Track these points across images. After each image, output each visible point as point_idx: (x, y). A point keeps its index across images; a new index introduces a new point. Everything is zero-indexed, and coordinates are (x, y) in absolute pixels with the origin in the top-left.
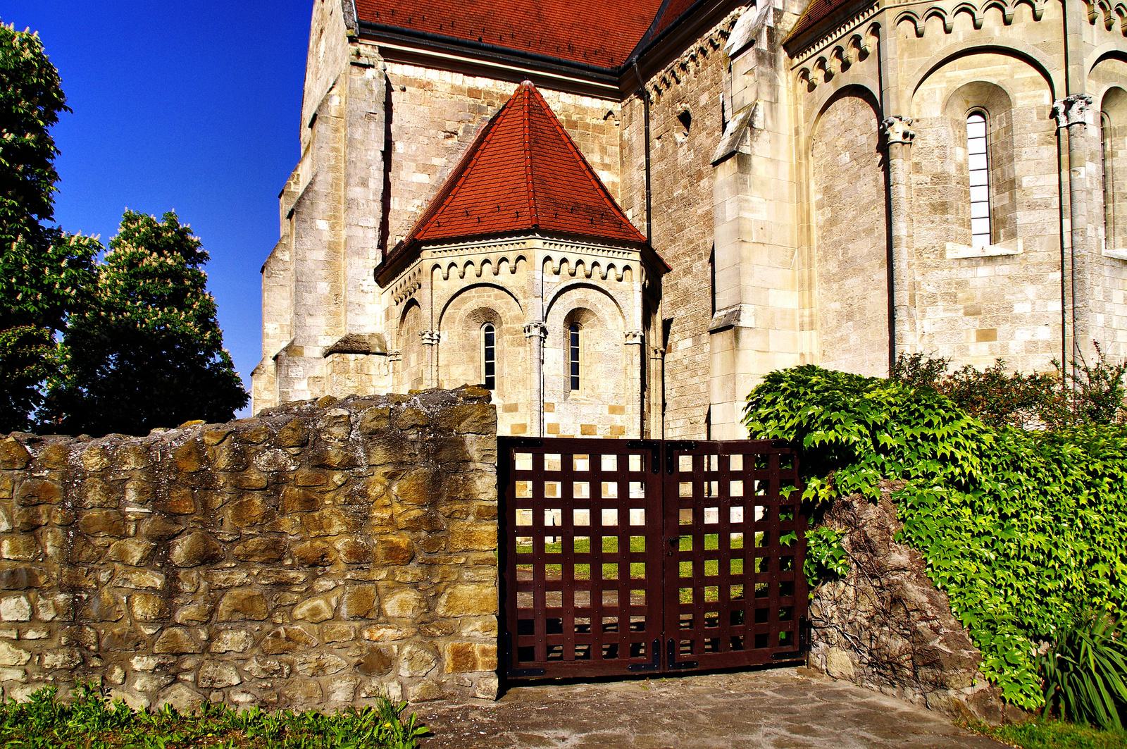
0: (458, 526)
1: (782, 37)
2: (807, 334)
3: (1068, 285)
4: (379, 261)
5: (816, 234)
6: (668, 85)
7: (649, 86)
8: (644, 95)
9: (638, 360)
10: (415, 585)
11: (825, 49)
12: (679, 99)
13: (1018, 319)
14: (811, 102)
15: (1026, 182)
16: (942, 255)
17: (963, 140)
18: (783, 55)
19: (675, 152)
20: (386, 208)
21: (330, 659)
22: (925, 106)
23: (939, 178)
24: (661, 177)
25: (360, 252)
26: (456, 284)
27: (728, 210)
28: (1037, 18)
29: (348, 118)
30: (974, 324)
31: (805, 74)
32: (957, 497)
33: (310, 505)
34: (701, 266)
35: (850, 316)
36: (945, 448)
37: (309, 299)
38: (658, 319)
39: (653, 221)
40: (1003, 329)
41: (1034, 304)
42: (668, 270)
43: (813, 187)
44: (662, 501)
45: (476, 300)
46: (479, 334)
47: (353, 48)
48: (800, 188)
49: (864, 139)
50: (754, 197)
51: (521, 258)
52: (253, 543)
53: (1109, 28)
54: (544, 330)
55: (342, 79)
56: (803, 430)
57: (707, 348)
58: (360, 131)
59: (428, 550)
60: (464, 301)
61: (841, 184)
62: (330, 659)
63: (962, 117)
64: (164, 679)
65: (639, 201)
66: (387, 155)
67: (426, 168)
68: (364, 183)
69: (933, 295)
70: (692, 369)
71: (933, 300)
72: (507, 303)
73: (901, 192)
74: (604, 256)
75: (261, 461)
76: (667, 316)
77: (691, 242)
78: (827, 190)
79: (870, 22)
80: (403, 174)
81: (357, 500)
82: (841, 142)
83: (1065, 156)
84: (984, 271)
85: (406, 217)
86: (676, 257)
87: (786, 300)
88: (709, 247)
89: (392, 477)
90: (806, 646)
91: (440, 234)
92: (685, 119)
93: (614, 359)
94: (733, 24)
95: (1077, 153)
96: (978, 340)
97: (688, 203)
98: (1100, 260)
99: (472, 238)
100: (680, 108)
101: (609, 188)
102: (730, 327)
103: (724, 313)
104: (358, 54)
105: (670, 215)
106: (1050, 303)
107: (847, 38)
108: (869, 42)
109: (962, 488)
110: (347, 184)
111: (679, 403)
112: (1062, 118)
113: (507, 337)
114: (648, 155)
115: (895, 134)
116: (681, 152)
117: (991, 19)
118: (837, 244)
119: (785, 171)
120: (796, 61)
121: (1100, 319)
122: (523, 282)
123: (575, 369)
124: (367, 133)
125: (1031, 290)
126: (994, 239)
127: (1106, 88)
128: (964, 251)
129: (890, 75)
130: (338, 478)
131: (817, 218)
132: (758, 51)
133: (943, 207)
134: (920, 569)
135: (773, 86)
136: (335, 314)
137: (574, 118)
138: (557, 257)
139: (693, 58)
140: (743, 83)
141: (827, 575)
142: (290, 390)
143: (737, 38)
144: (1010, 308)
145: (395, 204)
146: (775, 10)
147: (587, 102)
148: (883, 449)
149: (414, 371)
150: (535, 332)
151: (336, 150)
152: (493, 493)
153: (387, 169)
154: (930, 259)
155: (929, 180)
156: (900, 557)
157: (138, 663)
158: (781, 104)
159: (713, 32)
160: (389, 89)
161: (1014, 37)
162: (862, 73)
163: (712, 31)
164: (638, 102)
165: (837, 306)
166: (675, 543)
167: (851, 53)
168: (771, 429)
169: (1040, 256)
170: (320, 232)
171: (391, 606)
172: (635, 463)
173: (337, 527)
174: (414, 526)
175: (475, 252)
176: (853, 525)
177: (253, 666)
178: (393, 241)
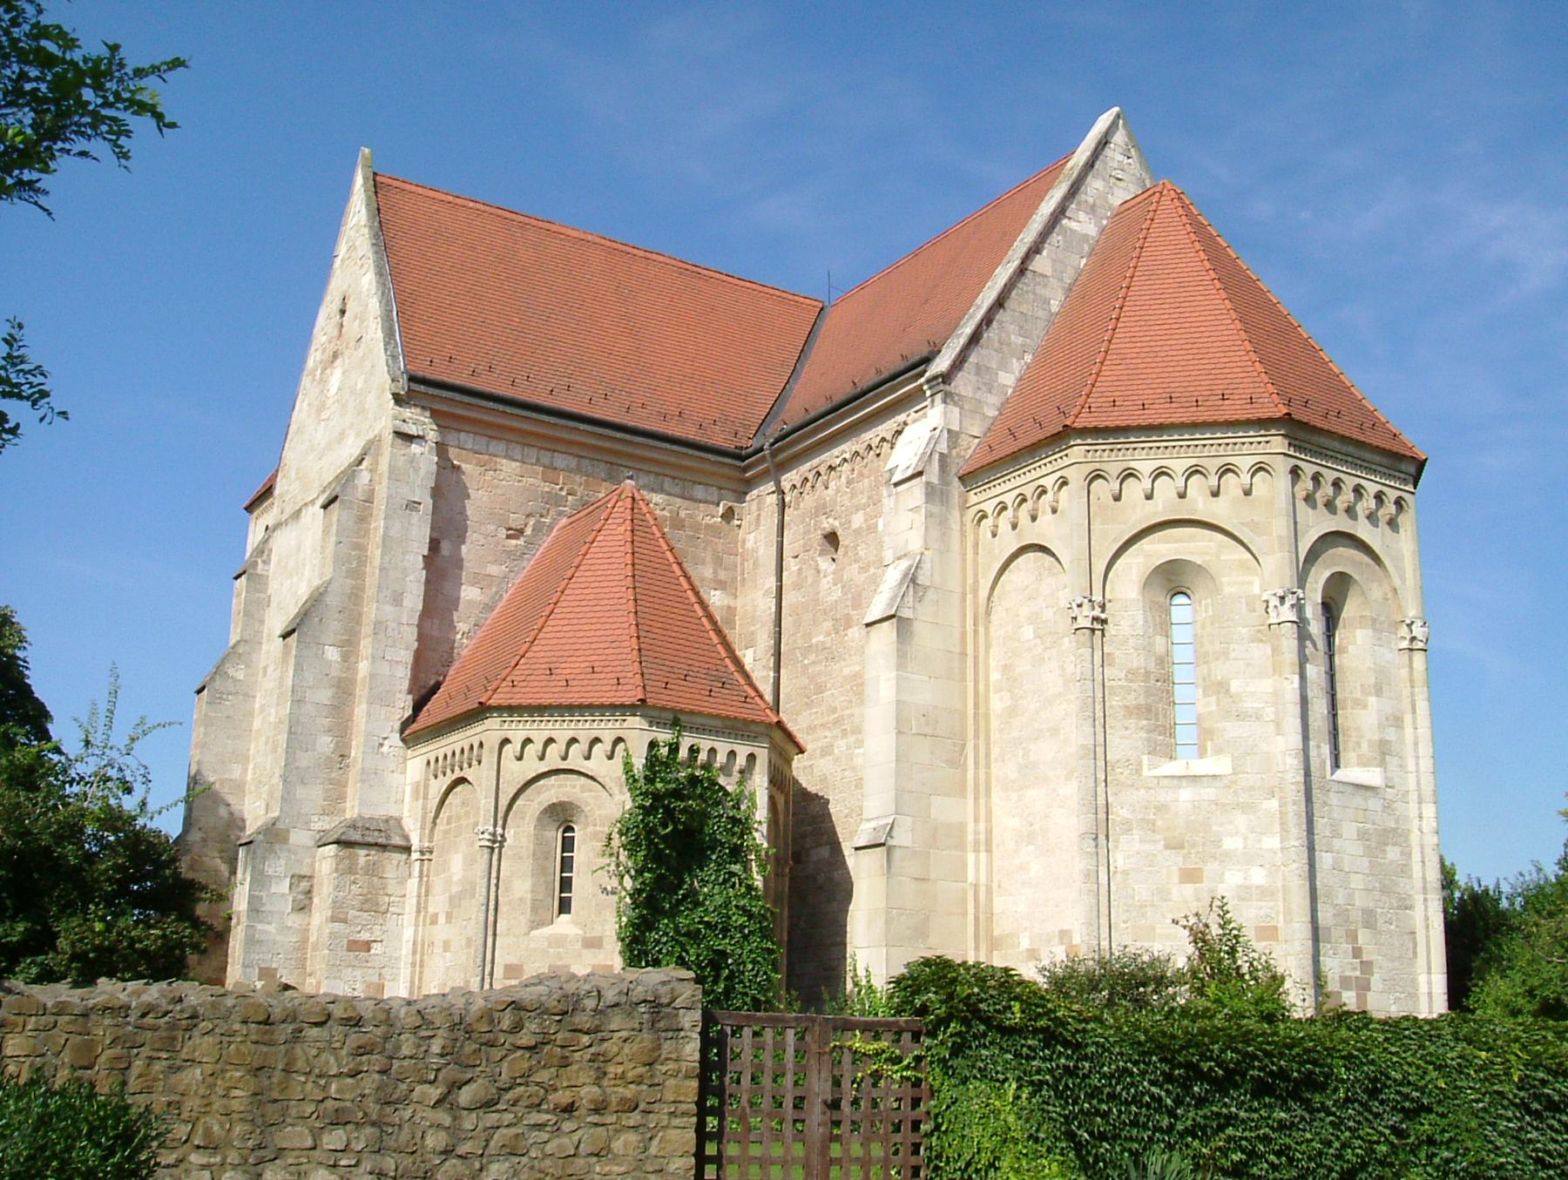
1: (958, 466)
12: (823, 509)
13: (1227, 856)
19: (816, 582)
40: (1210, 868)
41: (1245, 839)
51: (619, 740)
58: (398, 525)
65: (765, 641)
69: (1128, 821)
71: (1128, 827)
72: (596, 798)
77: (834, 710)
79: (1059, 474)
82: (1024, 611)
92: (832, 538)
96: (1182, 882)
100: (827, 524)
103: (873, 824)
105: (806, 667)
106: (1264, 838)
116: (825, 583)
125: (1241, 821)
142: (263, 894)
144: (1218, 843)
146: (949, 431)
152: (697, 1056)
155: (1123, 675)
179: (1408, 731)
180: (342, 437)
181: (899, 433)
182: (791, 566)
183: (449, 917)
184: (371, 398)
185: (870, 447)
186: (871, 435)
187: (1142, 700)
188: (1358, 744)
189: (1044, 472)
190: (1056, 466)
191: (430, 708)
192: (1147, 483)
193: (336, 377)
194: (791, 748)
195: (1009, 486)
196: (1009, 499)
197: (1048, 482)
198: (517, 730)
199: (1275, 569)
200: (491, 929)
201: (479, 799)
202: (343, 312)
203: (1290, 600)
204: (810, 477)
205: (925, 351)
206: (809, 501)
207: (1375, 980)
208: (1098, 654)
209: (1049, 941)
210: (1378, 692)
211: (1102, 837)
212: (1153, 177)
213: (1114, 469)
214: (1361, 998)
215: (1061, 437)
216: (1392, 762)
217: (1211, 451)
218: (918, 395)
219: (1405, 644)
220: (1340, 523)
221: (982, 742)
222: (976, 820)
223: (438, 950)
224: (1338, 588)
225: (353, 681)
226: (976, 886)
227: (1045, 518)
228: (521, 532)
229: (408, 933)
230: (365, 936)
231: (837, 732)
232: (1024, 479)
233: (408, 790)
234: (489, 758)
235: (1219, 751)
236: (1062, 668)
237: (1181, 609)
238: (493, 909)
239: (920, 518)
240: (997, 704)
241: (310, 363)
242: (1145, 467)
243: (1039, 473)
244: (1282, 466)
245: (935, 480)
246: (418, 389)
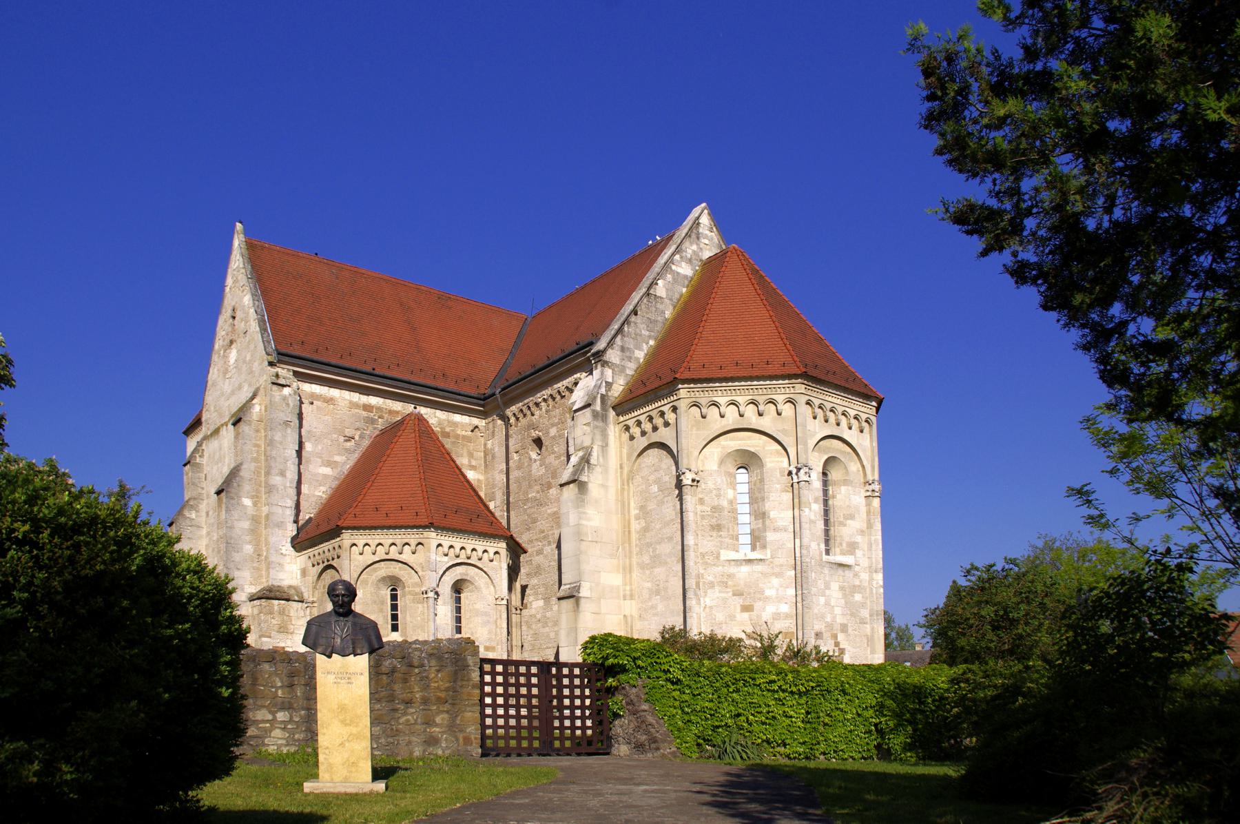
0: (465, 690)
2: (628, 602)
3: (799, 580)
4: (295, 533)
5: (634, 536)
6: (525, 416)
7: (509, 412)
8: (505, 419)
9: (505, 616)
10: (447, 712)
11: (641, 413)
12: (533, 426)
14: (631, 448)
15: (773, 514)
16: (718, 557)
17: (733, 485)
18: (612, 413)
19: (530, 465)
20: (299, 493)
21: (414, 739)
22: (707, 463)
23: (716, 509)
24: (518, 481)
25: (280, 525)
27: (572, 518)
28: (779, 414)
29: (268, 423)
30: (738, 601)
31: (627, 428)
32: (670, 686)
33: (405, 681)
34: (551, 550)
35: (658, 593)
36: (666, 667)
38: (518, 586)
39: (512, 513)
43: (632, 504)
44: (545, 686)
45: (384, 570)
46: (387, 593)
47: (273, 370)
48: (624, 506)
49: (667, 478)
50: (590, 511)
52: (382, 694)
53: (826, 421)
54: (437, 593)
55: (261, 392)
56: (607, 658)
57: (555, 608)
58: (279, 434)
59: (452, 699)
60: (375, 570)
61: (651, 506)
62: (414, 739)
63: (732, 469)
66: (299, 453)
67: (329, 464)
68: (282, 474)
69: (712, 583)
70: (544, 622)
71: (712, 585)
73: (690, 517)
74: (480, 545)
75: (387, 663)
76: (524, 583)
78: (642, 508)
80: (311, 467)
81: (425, 681)
82: (652, 478)
83: (796, 500)
84: (745, 569)
85: (314, 499)
86: (531, 541)
87: (614, 579)
88: (557, 537)
89: (438, 671)
90: (610, 746)
91: (356, 523)
92: (538, 442)
93: (486, 614)
94: (576, 384)
95: (803, 499)
97: (540, 504)
98: (821, 564)
99: (382, 528)
100: (535, 434)
101: (474, 484)
102: (572, 596)
104: (277, 376)
107: (656, 411)
108: (670, 417)
109: (673, 683)
110: (268, 473)
111: (533, 645)
112: (795, 477)
113: (409, 597)
114: (507, 464)
115: (687, 479)
117: (750, 411)
118: (649, 545)
119: (612, 493)
120: (621, 419)
121: (822, 600)
122: (421, 560)
123: (458, 620)
124: (284, 437)
125: (775, 581)
126: (753, 549)
127: (826, 457)
128: (733, 555)
129: (684, 441)
130: (417, 671)
131: (635, 526)
132: (594, 411)
133: (718, 527)
134: (653, 712)
135: (605, 436)
136: (258, 569)
137: (448, 430)
138: (446, 544)
139: (545, 400)
140: (582, 431)
141: (616, 716)
143: (578, 398)
144: (762, 592)
145: (305, 489)
147: (458, 418)
148: (639, 667)
150: (431, 594)
151: (258, 446)
153: (300, 463)
154: (710, 559)
156: (645, 707)
158: (612, 447)
159: (561, 385)
160: (301, 403)
161: (765, 423)
162: (665, 435)
163: (559, 385)
164: (499, 422)
165: (649, 585)
166: (551, 702)
167: (659, 421)
168: (591, 658)
169: (782, 561)
170: (245, 507)
171: (438, 720)
173: (416, 689)
174: (447, 690)
176: (626, 696)
177: (382, 740)
178: (304, 516)
180: (240, 387)
193: (233, 355)
202: (234, 318)
217: (761, 390)
227: (662, 430)
241: (216, 347)
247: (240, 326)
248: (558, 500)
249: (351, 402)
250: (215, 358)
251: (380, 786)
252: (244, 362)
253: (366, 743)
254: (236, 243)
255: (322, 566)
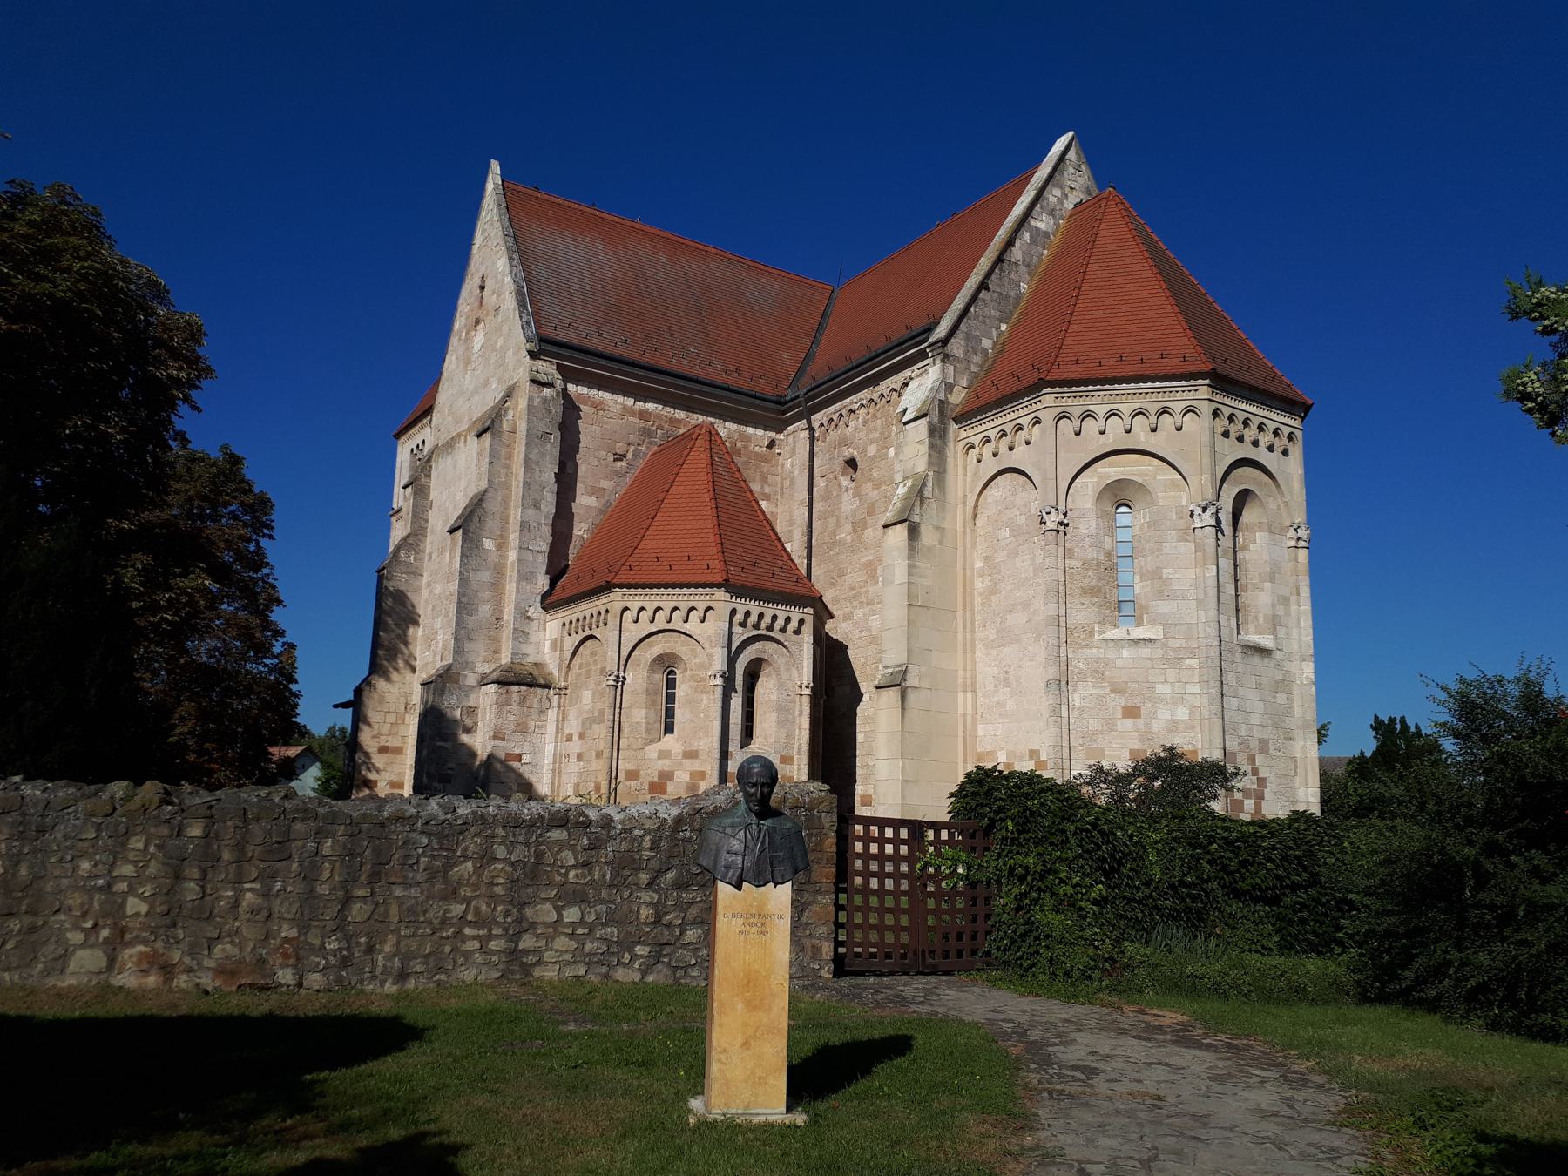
4: (546, 588)
12: (844, 442)
24: (822, 518)
26: (645, 628)
35: (1006, 683)
37: (471, 622)
42: (832, 617)
46: (660, 678)
51: (709, 608)
60: (651, 645)
64: (652, 961)
78: (987, 559)
92: (852, 463)
100: (848, 453)
107: (1288, 430)
149: (587, 708)
152: (834, 849)
157: (639, 950)
172: (904, 834)
175: (666, 600)
179: (1293, 608)
180: (486, 383)
181: (906, 385)
182: (820, 484)
183: (581, 736)
184: (510, 353)
185: (882, 396)
186: (885, 386)
187: (1094, 583)
188: (1256, 618)
189: (1021, 413)
190: (1031, 409)
191: (566, 582)
192: (1101, 421)
193: (479, 338)
194: (825, 615)
195: (992, 424)
196: (992, 434)
197: (1024, 421)
198: (635, 600)
199: (1202, 483)
200: (616, 745)
201: (607, 651)
202: (482, 288)
203: (1212, 510)
204: (835, 417)
205: (926, 322)
206: (833, 435)
207: (1267, 792)
208: (1061, 549)
209: (1021, 757)
210: (1272, 579)
211: (1063, 683)
212: (1101, 188)
213: (1076, 412)
214: (1258, 808)
215: (1034, 389)
216: (1281, 632)
217: (1153, 395)
218: (922, 355)
219: (1293, 543)
220: (1246, 451)
221: (968, 615)
222: (964, 670)
223: (573, 759)
224: (1243, 498)
225: (504, 566)
226: (965, 715)
227: (1021, 448)
228: (624, 456)
229: (550, 748)
230: (517, 751)
231: (856, 603)
232: (1004, 420)
233: (548, 644)
234: (613, 621)
235: (1152, 622)
236: (1033, 559)
237: (1123, 516)
238: (617, 731)
239: (924, 449)
240: (980, 584)
241: (457, 326)
242: (1101, 410)
243: (1017, 414)
244: (1206, 409)
245: (936, 420)
246: (543, 346)
247: (490, 298)
248: (879, 544)
249: (624, 407)
250: (454, 342)
251: (800, 1118)
252: (495, 350)
253: (782, 1043)
254: (490, 186)
255: (581, 636)
